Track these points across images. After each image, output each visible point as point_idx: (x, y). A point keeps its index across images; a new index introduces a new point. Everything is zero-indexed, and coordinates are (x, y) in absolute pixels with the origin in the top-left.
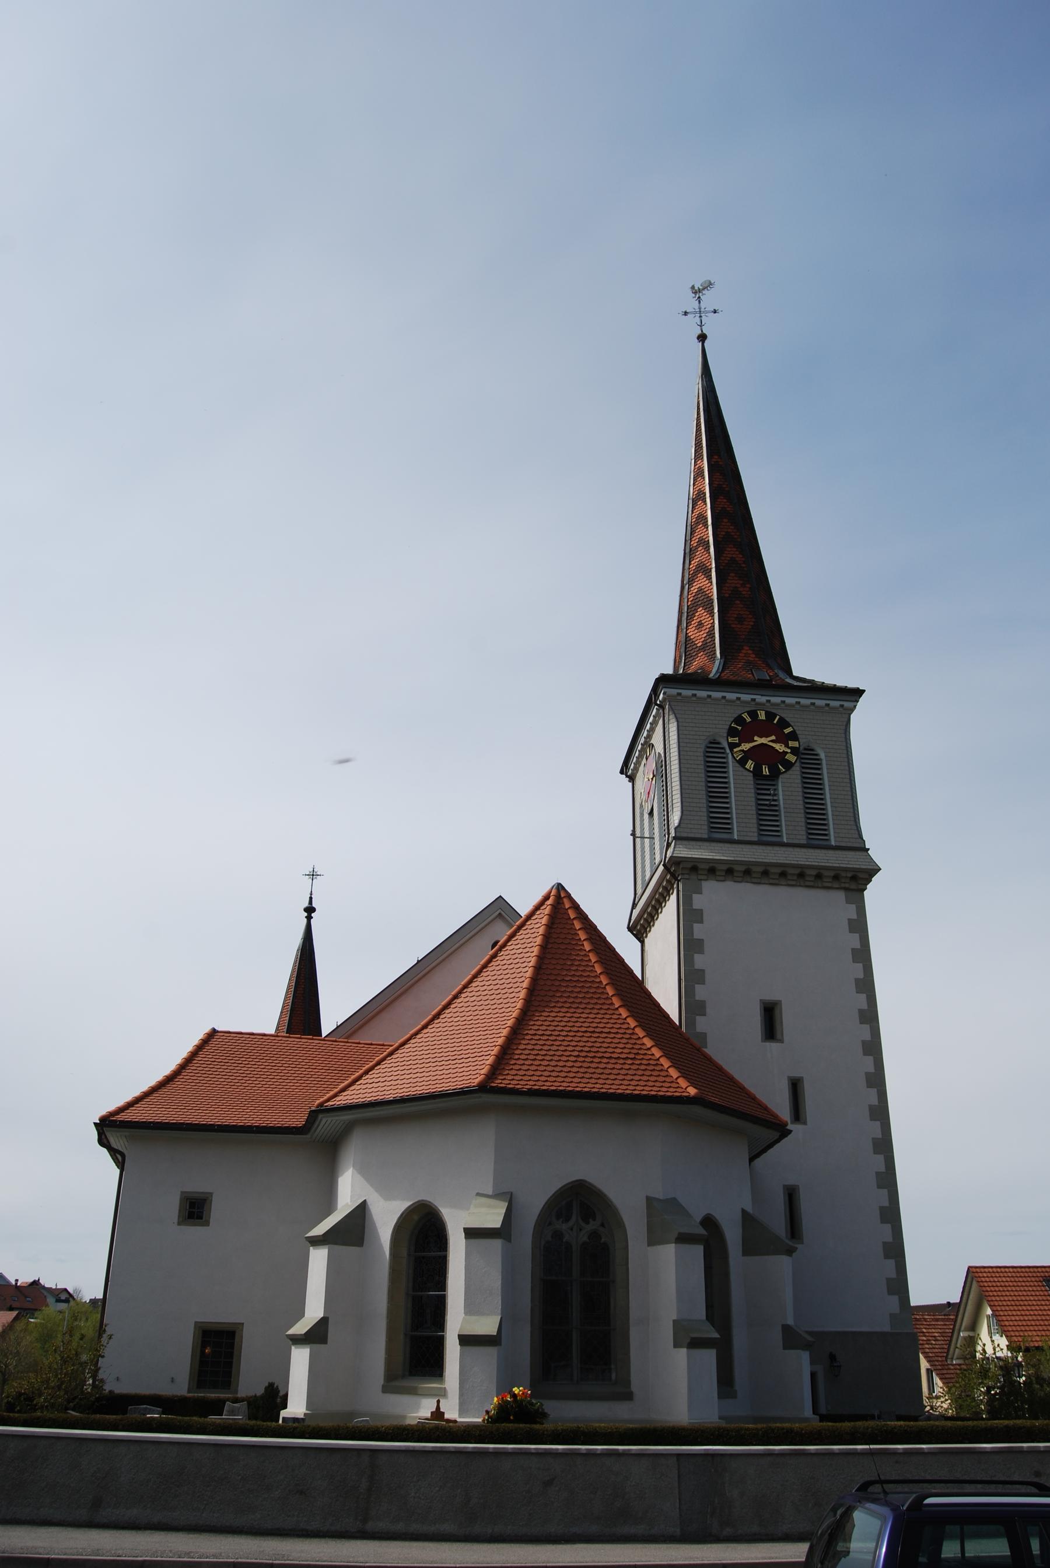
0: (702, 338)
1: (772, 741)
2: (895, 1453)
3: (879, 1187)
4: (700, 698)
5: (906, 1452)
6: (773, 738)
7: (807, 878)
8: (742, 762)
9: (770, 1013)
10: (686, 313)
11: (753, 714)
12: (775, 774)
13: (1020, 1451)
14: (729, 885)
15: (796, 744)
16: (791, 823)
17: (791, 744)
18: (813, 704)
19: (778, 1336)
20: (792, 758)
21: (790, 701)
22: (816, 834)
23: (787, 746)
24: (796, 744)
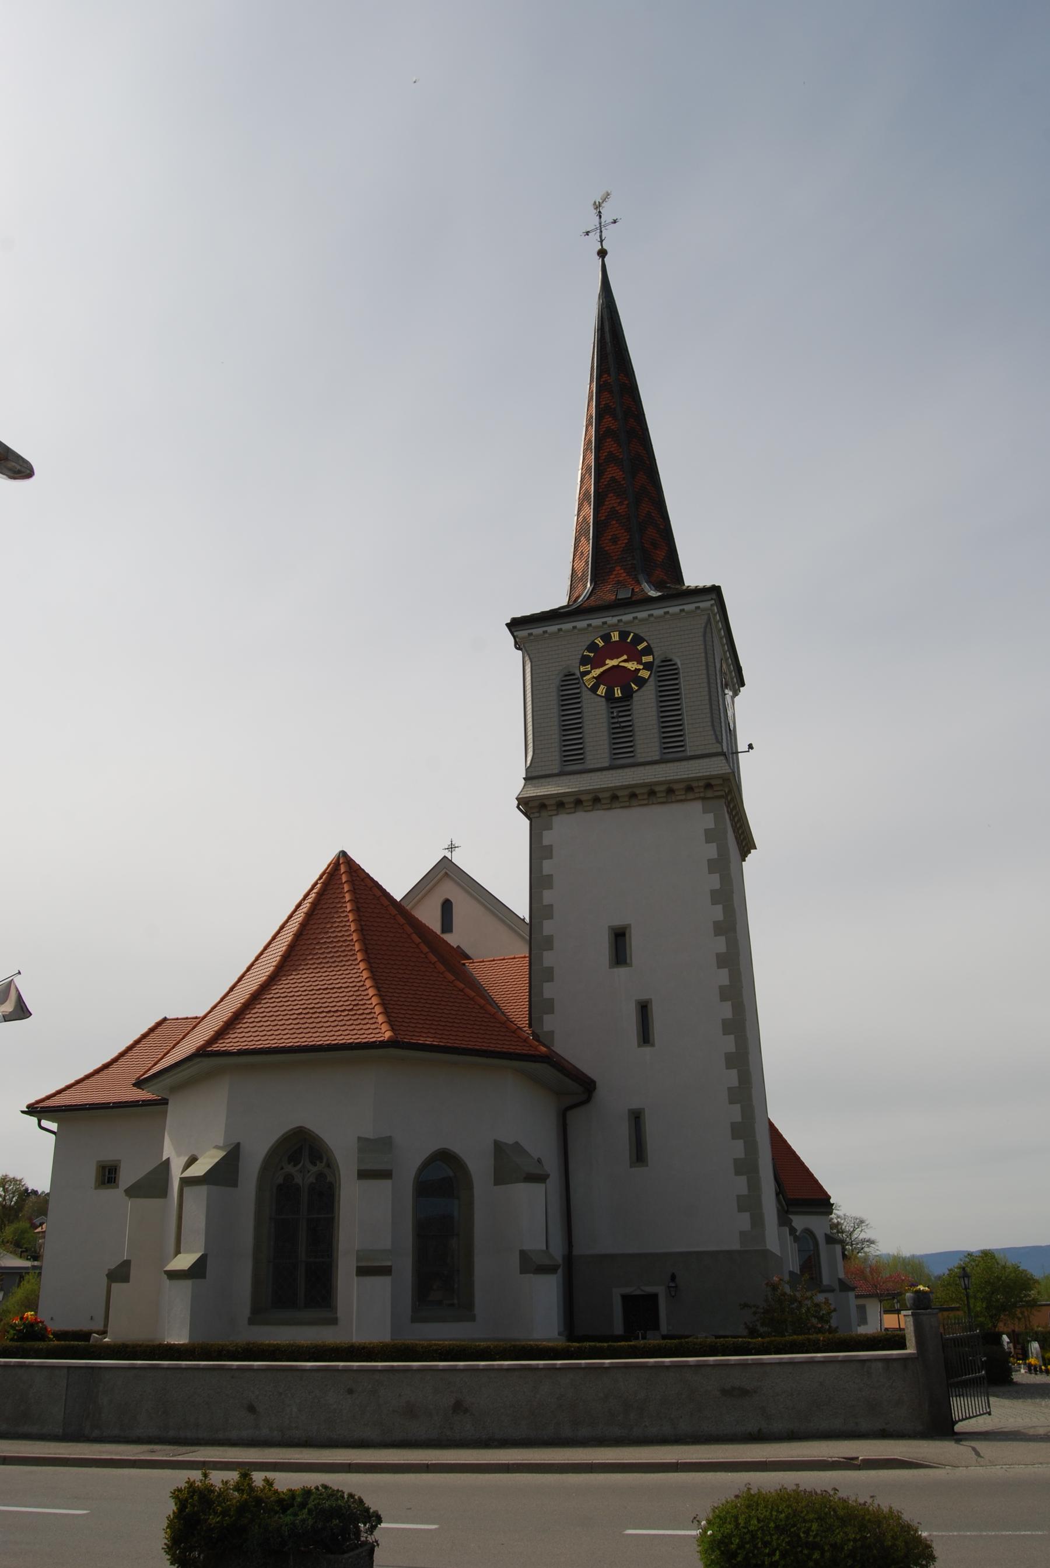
0: (602, 253)
1: (625, 661)
2: (229, 1369)
3: (731, 1102)
5: (240, 1369)
6: (625, 657)
7: (659, 795)
8: (594, 689)
9: (620, 937)
10: (615, 222)
11: (606, 638)
12: (628, 695)
13: (336, 1370)
14: (581, 816)
15: (650, 659)
17: (645, 659)
18: (636, 618)
19: (515, 1261)
20: (645, 674)
22: (673, 744)
23: (640, 662)
24: (650, 659)
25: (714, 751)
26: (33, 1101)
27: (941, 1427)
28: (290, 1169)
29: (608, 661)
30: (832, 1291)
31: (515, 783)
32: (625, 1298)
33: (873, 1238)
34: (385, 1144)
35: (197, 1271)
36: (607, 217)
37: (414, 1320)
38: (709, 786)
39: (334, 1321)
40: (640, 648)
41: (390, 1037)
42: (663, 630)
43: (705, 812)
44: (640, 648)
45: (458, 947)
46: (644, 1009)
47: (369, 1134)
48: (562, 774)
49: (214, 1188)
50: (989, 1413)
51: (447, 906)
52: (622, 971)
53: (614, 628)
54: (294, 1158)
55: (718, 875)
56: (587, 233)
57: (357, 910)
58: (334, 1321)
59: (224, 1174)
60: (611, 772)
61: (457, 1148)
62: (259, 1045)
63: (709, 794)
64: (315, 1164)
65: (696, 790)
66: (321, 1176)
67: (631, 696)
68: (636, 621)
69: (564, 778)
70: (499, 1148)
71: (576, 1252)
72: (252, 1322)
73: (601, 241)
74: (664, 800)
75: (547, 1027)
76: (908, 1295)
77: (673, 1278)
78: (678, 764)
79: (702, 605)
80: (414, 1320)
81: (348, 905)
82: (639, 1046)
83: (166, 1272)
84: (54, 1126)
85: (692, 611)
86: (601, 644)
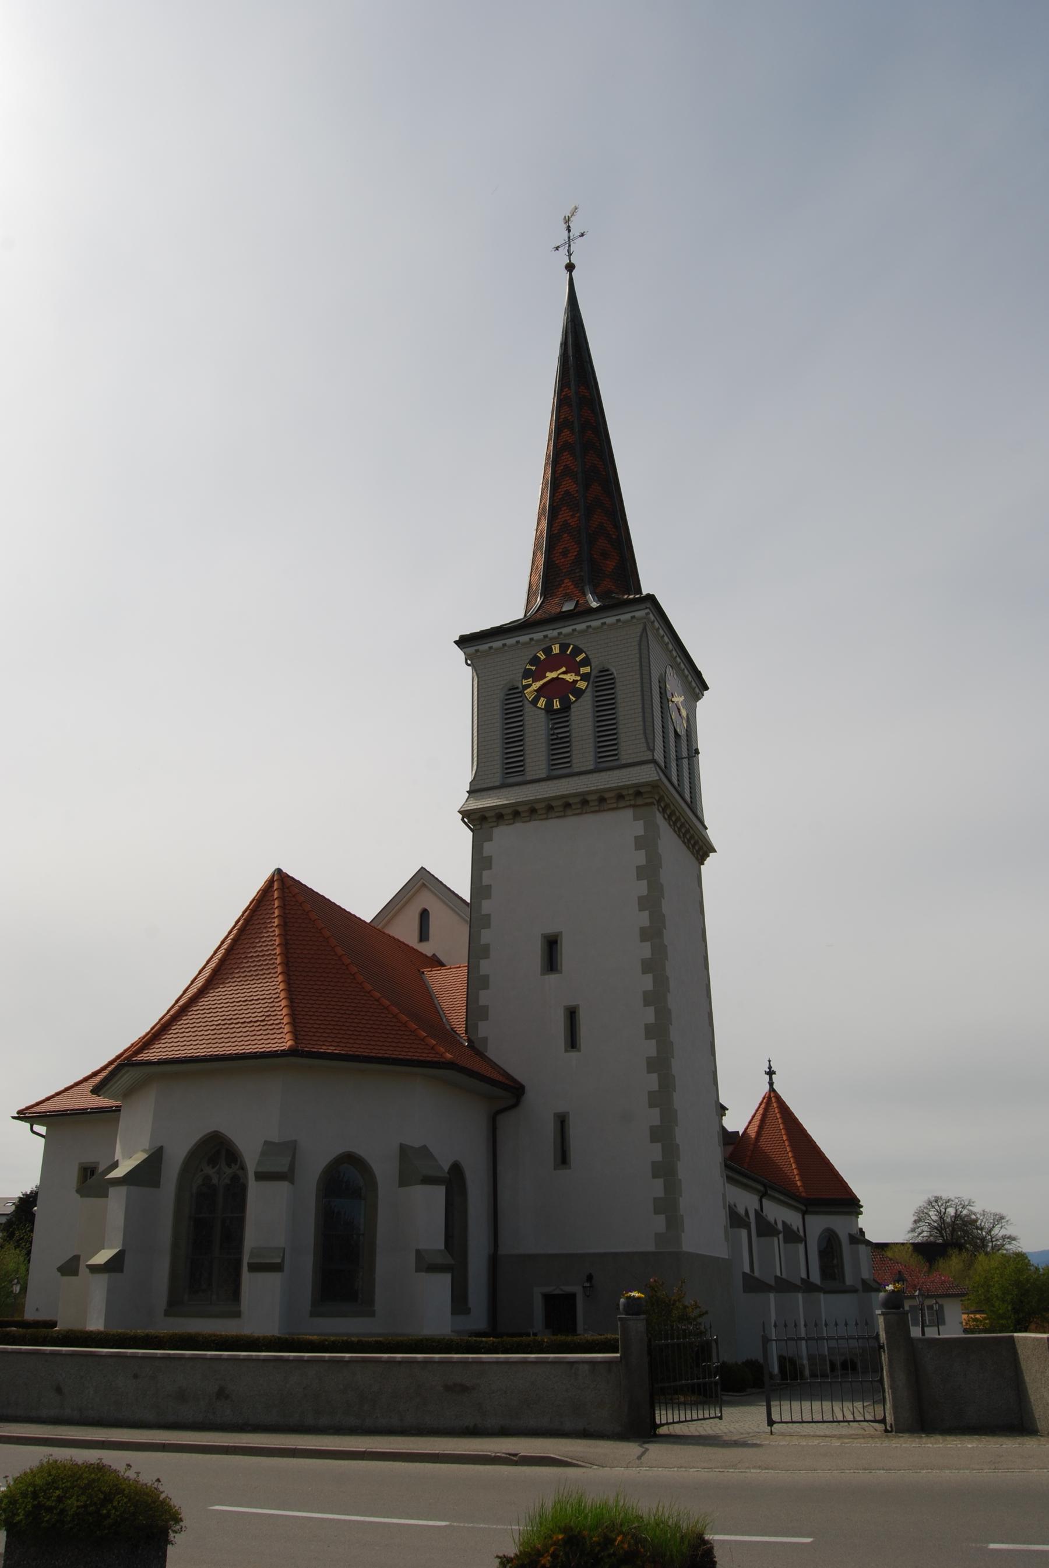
0: (570, 267)
1: (564, 673)
3: (651, 1106)
4: (497, 649)
6: (564, 669)
9: (552, 945)
10: (582, 235)
11: (548, 651)
12: (566, 707)
14: (519, 826)
15: (587, 669)
16: (583, 752)
17: (583, 670)
20: (582, 685)
21: (581, 627)
23: (578, 674)
24: (587, 669)
25: (645, 758)
26: (23, 1107)
27: (643, 1430)
28: (209, 1171)
29: (548, 674)
30: (856, 1291)
31: (459, 797)
32: (548, 1298)
33: (1014, 1234)
34: (291, 1148)
35: (114, 1265)
36: (575, 232)
37: (313, 1314)
38: (638, 794)
39: (238, 1314)
40: (578, 659)
41: (290, 1046)
42: (605, 642)
43: (636, 819)
44: (578, 659)
45: (434, 955)
46: (572, 1015)
47: (275, 1138)
48: (548, 778)
49: (131, 1187)
50: (721, 1418)
51: (424, 915)
52: (553, 977)
53: (554, 640)
54: (213, 1161)
55: (645, 882)
56: (557, 248)
57: (284, 925)
58: (238, 1314)
59: (146, 1175)
60: (549, 783)
61: (361, 1151)
62: (177, 1054)
63: (640, 801)
64: (229, 1166)
65: (627, 798)
66: (235, 1178)
67: (569, 708)
68: (590, 630)
69: (504, 790)
70: (404, 1151)
71: (503, 1251)
72: (167, 1314)
73: (570, 255)
74: (597, 808)
75: (481, 1034)
76: (622, 1300)
77: (590, 1278)
78: (609, 773)
79: (637, 614)
80: (313, 1314)
81: (276, 920)
82: (566, 1051)
83: (89, 1266)
84: (42, 1129)
85: (598, 628)
86: (542, 656)
